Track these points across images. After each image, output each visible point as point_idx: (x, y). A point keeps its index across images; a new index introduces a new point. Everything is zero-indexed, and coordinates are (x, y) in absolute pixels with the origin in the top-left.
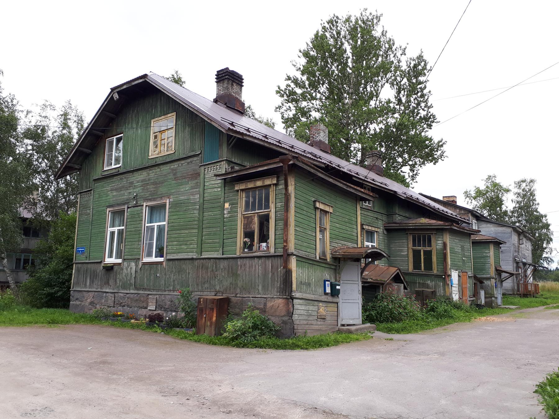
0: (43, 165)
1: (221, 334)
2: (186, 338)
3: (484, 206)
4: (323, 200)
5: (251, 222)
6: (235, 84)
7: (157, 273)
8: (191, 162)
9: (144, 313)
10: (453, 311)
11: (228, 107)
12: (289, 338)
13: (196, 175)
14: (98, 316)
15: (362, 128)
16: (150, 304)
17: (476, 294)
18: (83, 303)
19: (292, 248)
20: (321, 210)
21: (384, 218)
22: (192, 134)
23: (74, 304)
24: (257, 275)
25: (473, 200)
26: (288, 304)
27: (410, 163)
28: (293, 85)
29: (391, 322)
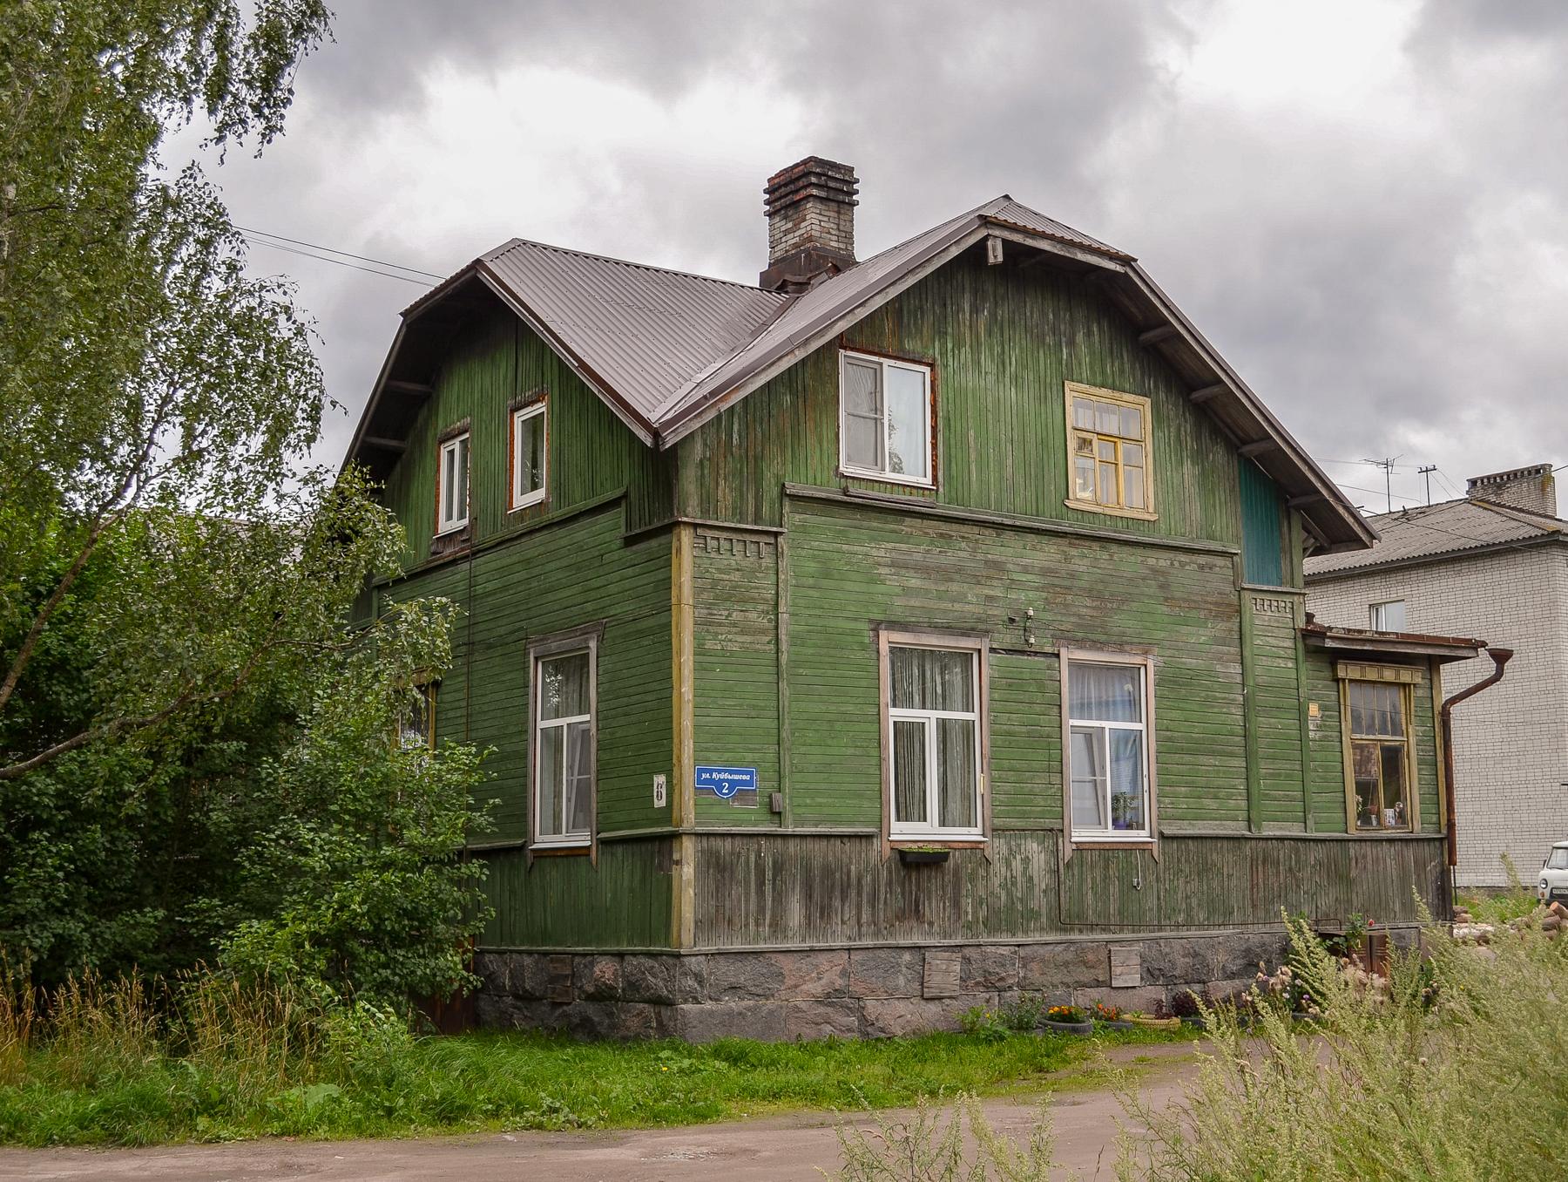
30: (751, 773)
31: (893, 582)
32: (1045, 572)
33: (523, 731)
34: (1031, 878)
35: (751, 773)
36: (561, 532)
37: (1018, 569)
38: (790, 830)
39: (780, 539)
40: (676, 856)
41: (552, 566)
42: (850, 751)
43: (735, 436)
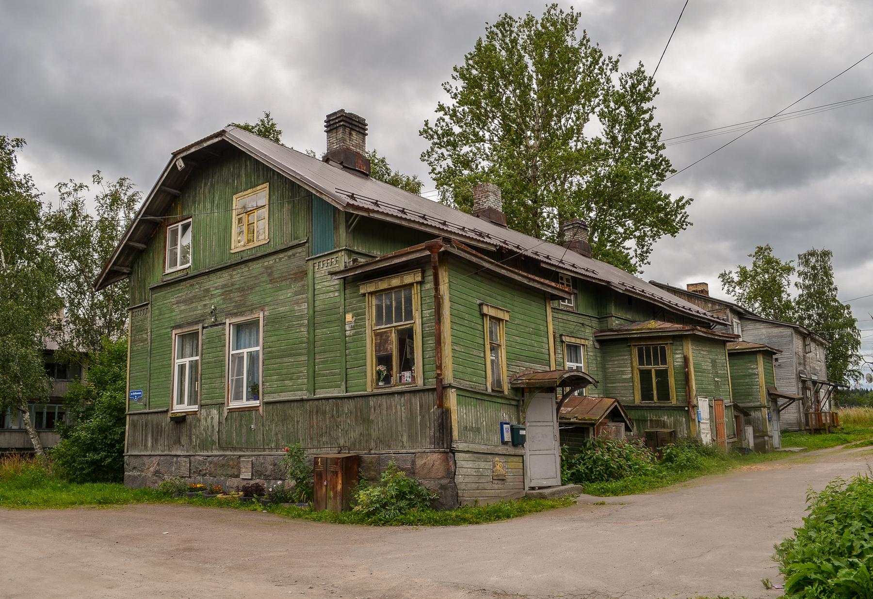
0: (72, 268)
1: (351, 509)
2: (299, 516)
3: (750, 299)
4: (493, 301)
5: (386, 341)
6: (354, 133)
7: (251, 423)
8: (294, 255)
9: (236, 485)
10: (699, 459)
11: (345, 168)
12: (451, 509)
13: (302, 274)
14: (168, 491)
15: (558, 182)
16: (243, 470)
17: (739, 433)
18: (144, 474)
19: (449, 377)
20: (492, 317)
21: (595, 323)
22: (294, 213)
23: (130, 476)
24: (399, 421)
25: (737, 287)
26: (446, 460)
27: (637, 234)
28: (447, 118)
29: (607, 481)
32: (223, 286)
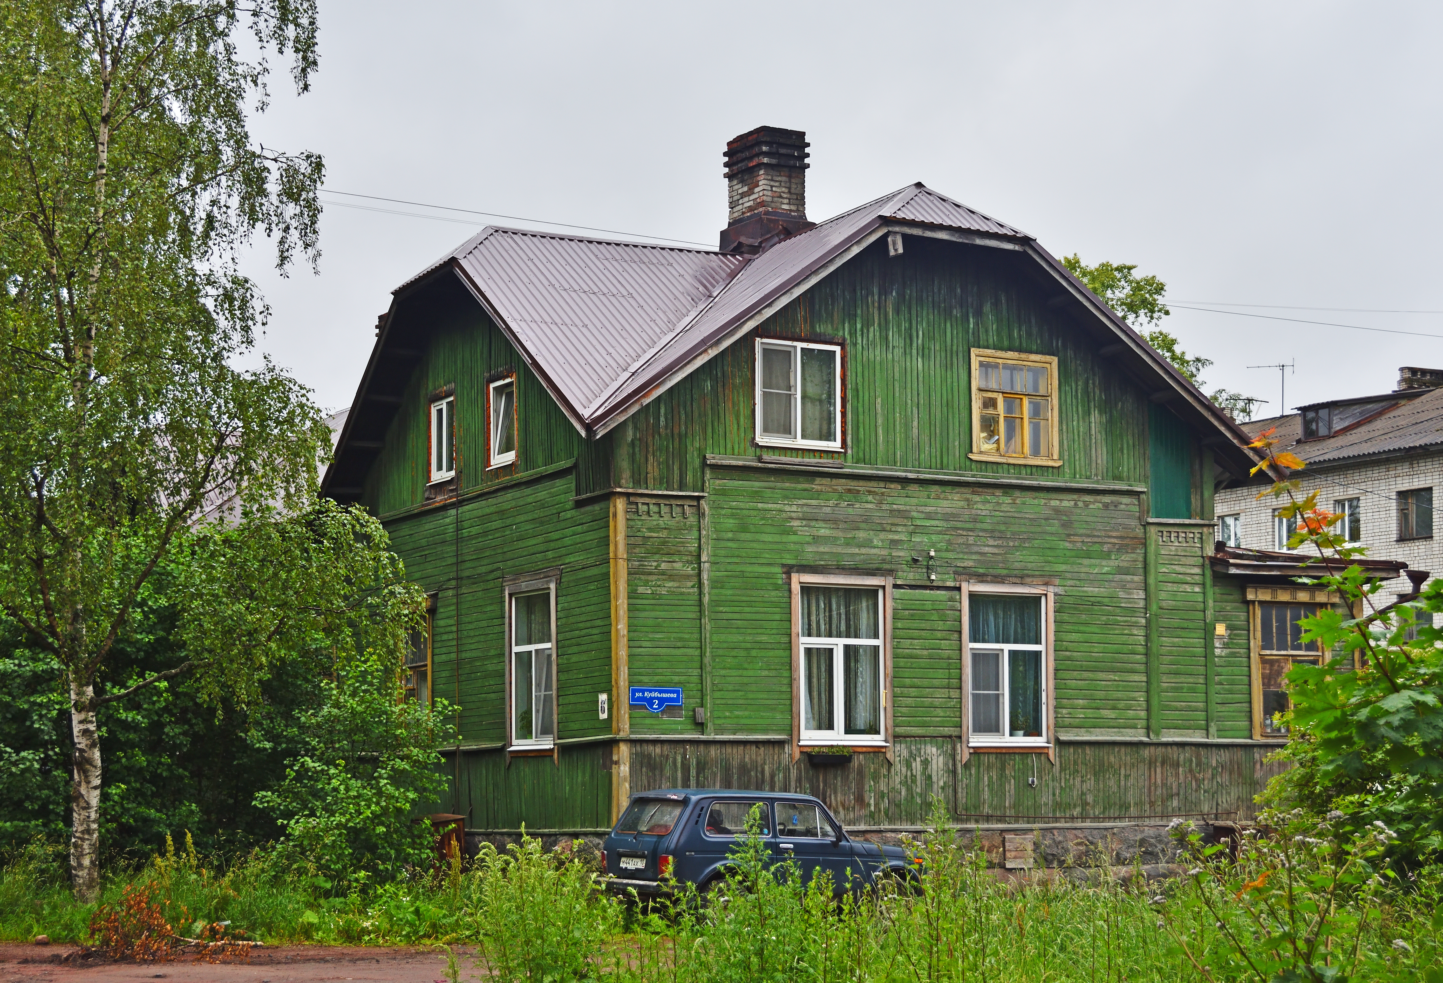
22: (1110, 428)
30: (677, 692)
31: (803, 531)
32: (947, 517)
33: (502, 655)
34: (930, 777)
35: (677, 692)
36: (528, 491)
37: (922, 516)
38: (712, 737)
39: (702, 502)
40: (615, 758)
41: (522, 518)
42: (765, 673)
43: (662, 419)
